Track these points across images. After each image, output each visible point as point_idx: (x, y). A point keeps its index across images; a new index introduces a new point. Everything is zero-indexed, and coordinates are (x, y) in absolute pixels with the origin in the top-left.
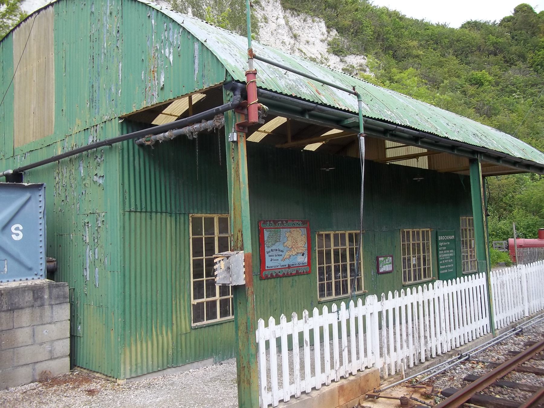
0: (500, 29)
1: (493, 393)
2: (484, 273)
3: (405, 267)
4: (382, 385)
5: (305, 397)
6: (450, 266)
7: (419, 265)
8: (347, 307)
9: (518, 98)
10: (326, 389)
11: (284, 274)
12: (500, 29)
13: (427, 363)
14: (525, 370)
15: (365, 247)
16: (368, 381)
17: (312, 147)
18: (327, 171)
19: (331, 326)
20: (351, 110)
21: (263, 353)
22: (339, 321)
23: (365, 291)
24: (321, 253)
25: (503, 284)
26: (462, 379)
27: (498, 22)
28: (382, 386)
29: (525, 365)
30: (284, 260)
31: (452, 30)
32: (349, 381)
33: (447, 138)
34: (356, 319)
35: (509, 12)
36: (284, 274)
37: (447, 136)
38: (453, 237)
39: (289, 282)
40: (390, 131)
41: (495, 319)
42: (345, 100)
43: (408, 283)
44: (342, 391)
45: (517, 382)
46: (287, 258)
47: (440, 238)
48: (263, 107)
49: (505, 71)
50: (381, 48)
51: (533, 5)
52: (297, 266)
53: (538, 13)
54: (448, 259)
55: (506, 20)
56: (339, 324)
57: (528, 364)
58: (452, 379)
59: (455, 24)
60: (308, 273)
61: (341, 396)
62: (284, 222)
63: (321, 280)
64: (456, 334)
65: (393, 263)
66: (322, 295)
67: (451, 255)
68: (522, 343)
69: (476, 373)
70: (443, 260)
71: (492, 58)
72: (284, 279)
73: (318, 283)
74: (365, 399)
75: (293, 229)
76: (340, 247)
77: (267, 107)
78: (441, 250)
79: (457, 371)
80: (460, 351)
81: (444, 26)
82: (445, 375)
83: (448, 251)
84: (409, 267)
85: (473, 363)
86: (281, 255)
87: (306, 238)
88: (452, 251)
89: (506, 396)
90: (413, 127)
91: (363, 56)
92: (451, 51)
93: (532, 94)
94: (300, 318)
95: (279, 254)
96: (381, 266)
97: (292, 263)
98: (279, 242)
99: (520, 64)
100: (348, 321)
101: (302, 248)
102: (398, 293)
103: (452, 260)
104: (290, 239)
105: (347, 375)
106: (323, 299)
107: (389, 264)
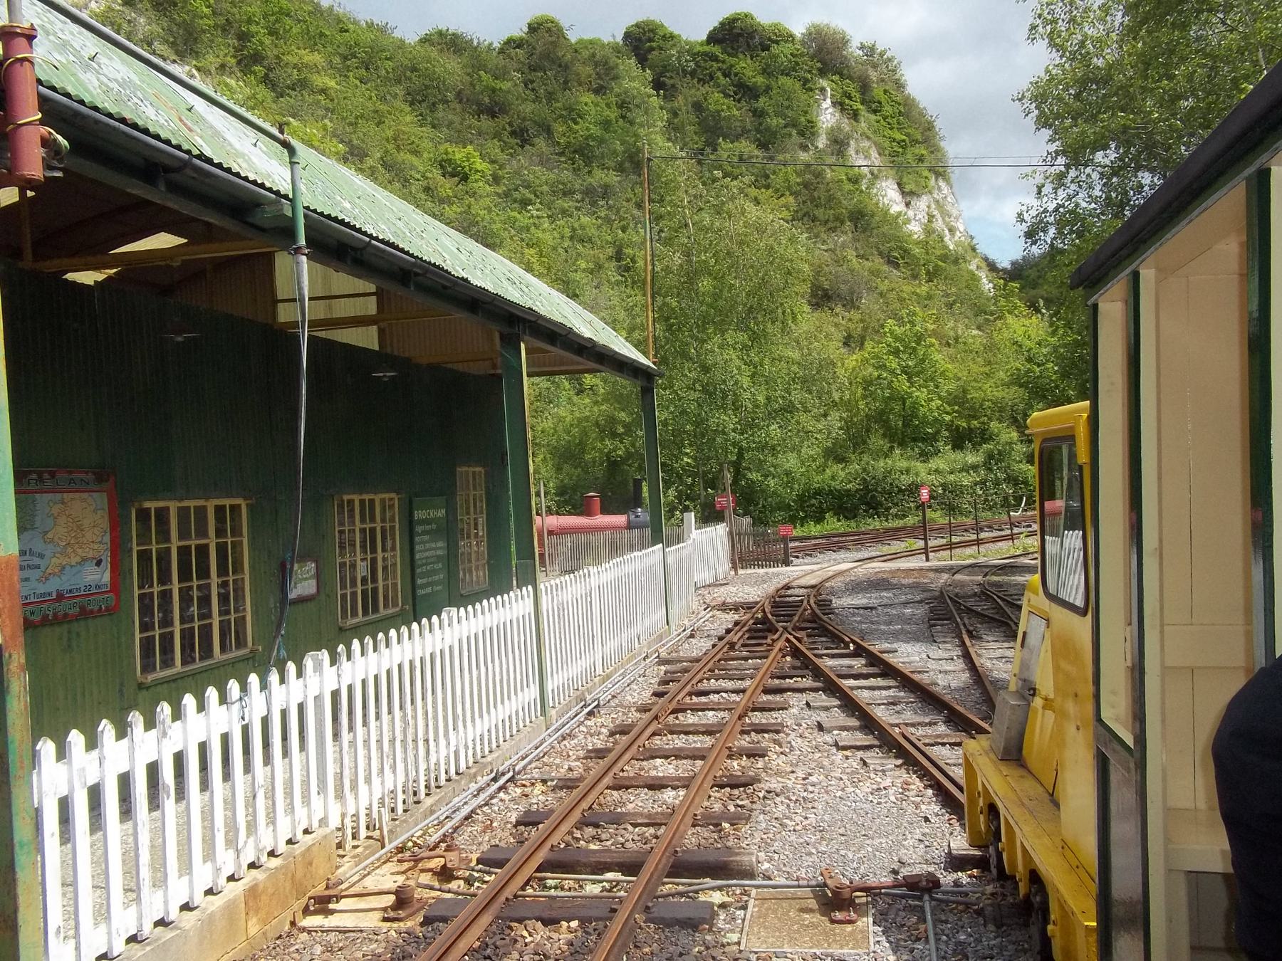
0: (501, 61)
1: (582, 842)
2: (530, 588)
4: (339, 867)
5: (166, 934)
7: (374, 580)
8: (264, 686)
9: (538, 217)
10: (216, 902)
11: (45, 617)
12: (501, 61)
13: (428, 802)
14: (627, 783)
15: (254, 538)
16: (311, 864)
17: (88, 278)
18: (178, 343)
19: (225, 739)
20: (268, 185)
21: (53, 834)
22: (244, 723)
23: (255, 647)
24: (144, 557)
25: (561, 607)
26: (511, 823)
27: (496, 45)
28: (341, 870)
29: (625, 774)
30: (47, 579)
31: (401, 44)
32: (268, 873)
33: (466, 280)
34: (284, 714)
35: (518, 29)
36: (45, 617)
37: (465, 276)
39: (60, 638)
40: (353, 249)
41: (550, 686)
43: (351, 622)
44: (255, 898)
45: (619, 810)
46: (54, 574)
47: (418, 515)
48: (55, 140)
49: (511, 155)
50: (235, 57)
51: (564, 23)
52: (32, 600)
53: (573, 41)
55: (512, 43)
56: (246, 730)
57: (630, 771)
58: (488, 827)
59: (409, 31)
60: (111, 611)
61: (251, 913)
62: (46, 476)
63: (145, 627)
64: (482, 726)
65: (318, 576)
66: (148, 667)
68: (604, 731)
69: (536, 806)
70: (423, 565)
71: (486, 123)
72: (47, 631)
73: (138, 636)
74: (306, 911)
75: (71, 495)
76: (193, 543)
77: (66, 143)
78: (420, 543)
79: (496, 808)
80: (491, 763)
81: (383, 30)
82: (473, 822)
85: (524, 786)
86: (38, 567)
87: (106, 518)
89: (609, 843)
90: (401, 246)
91: (187, 68)
92: (399, 90)
93: (565, 212)
94: (122, 731)
95: (31, 563)
97: (66, 587)
98: (30, 532)
99: (541, 143)
100: (266, 722)
101: (96, 546)
102: (371, 642)
104: (62, 520)
105: (264, 858)
106: (150, 677)
107: (310, 578)
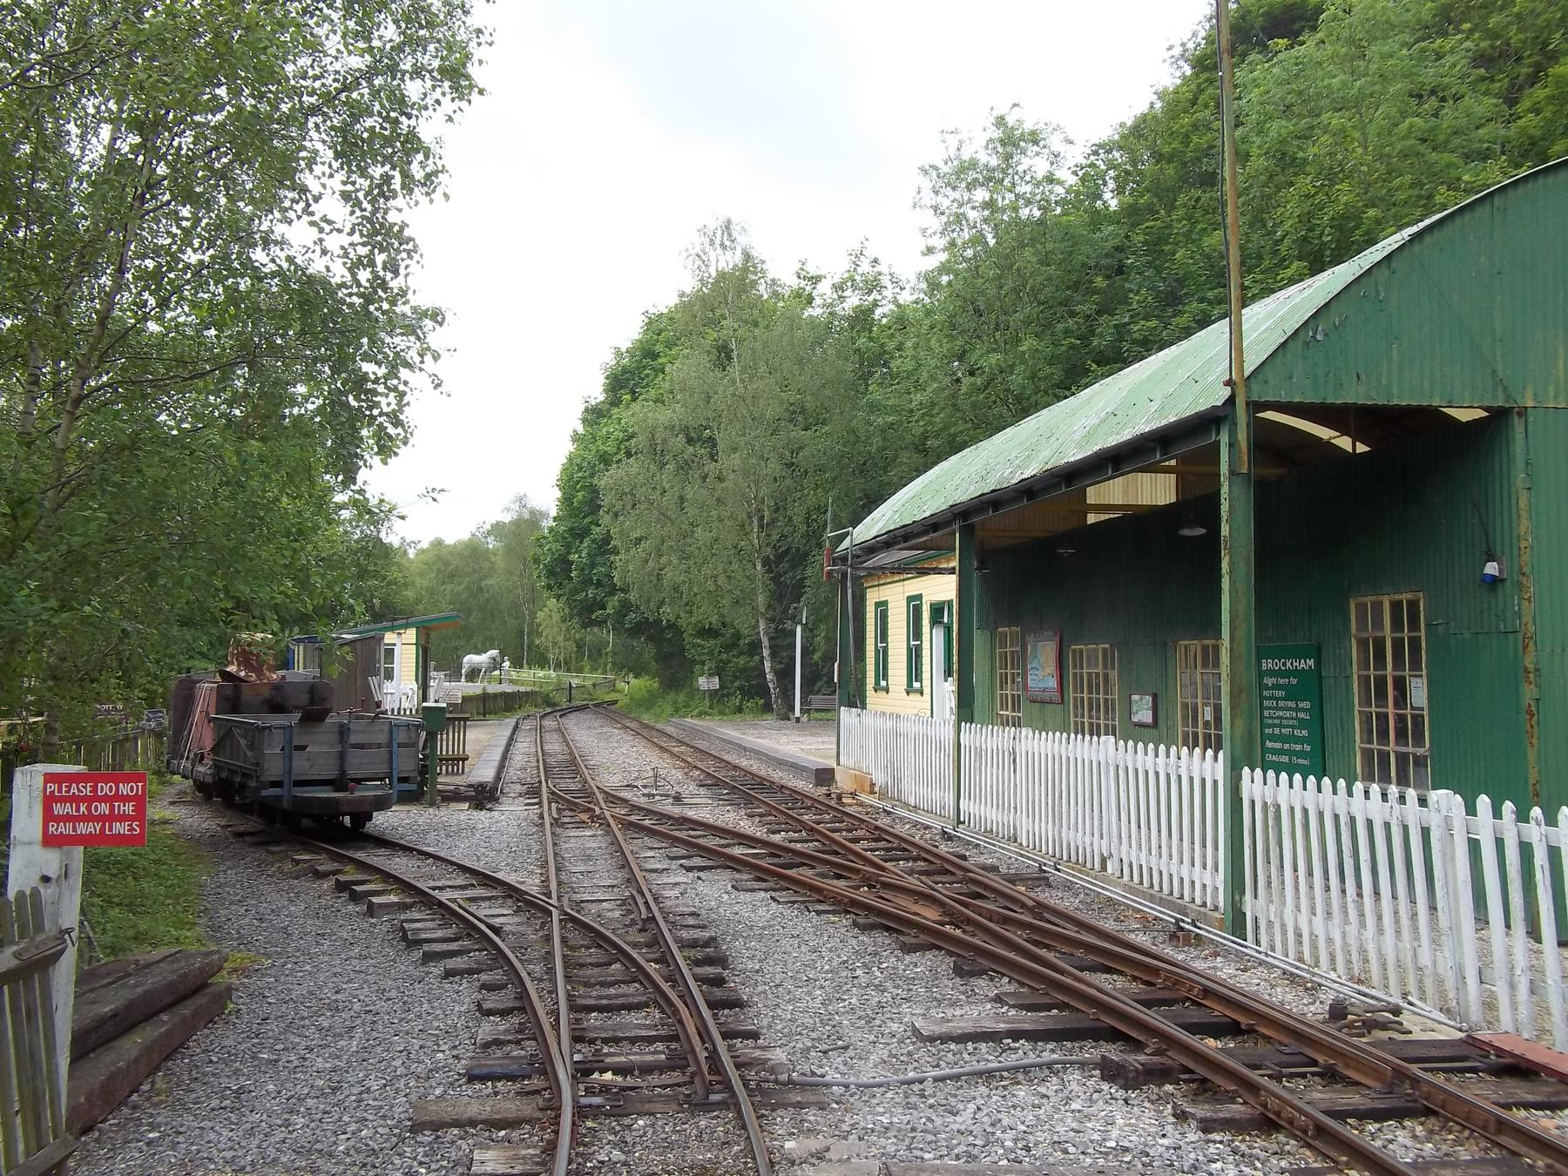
3: (1185, 725)
6: (1298, 747)
38: (1311, 662)
42: (595, 728)
54: (1293, 727)
67: (1301, 715)
83: (1291, 704)
84: (1195, 724)
88: (1306, 705)
96: (1134, 709)
103: (1305, 733)
